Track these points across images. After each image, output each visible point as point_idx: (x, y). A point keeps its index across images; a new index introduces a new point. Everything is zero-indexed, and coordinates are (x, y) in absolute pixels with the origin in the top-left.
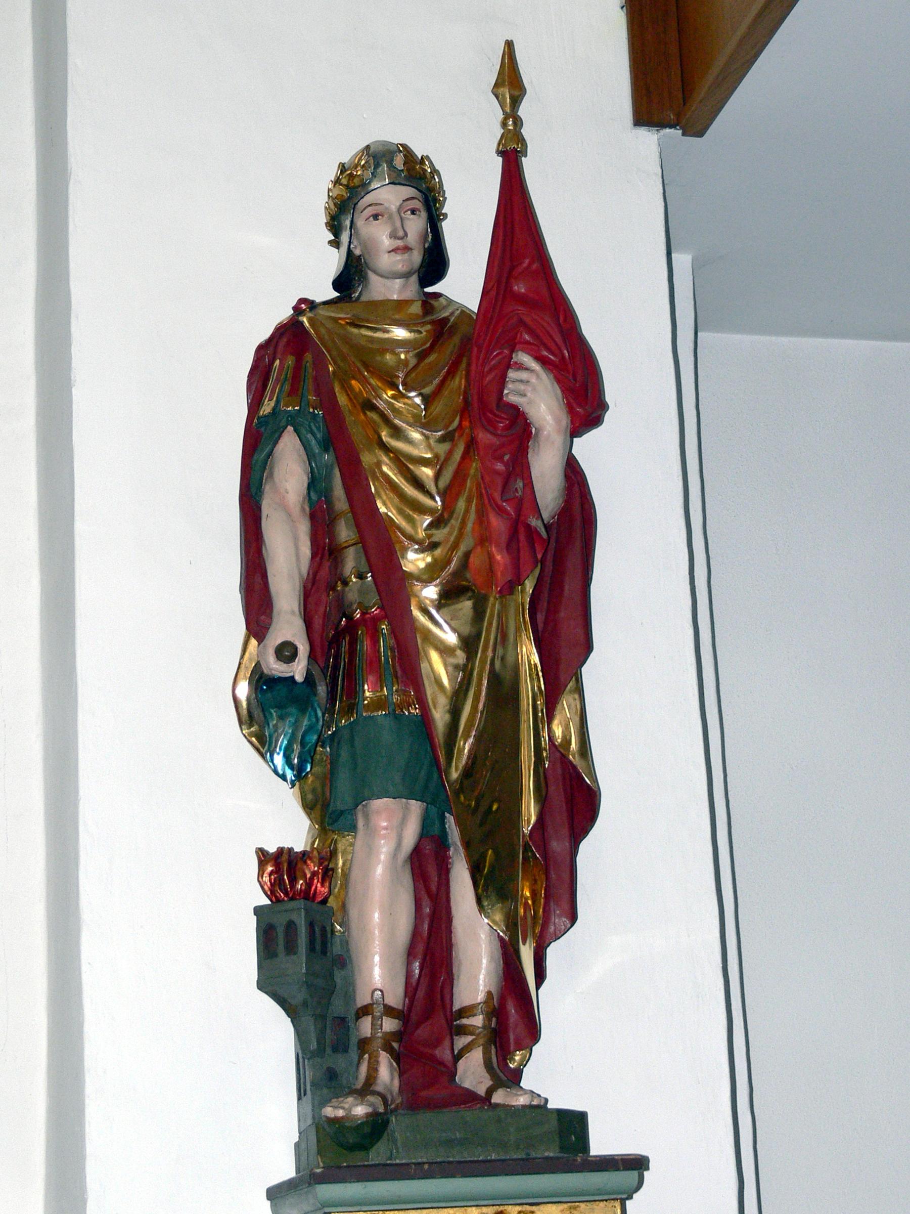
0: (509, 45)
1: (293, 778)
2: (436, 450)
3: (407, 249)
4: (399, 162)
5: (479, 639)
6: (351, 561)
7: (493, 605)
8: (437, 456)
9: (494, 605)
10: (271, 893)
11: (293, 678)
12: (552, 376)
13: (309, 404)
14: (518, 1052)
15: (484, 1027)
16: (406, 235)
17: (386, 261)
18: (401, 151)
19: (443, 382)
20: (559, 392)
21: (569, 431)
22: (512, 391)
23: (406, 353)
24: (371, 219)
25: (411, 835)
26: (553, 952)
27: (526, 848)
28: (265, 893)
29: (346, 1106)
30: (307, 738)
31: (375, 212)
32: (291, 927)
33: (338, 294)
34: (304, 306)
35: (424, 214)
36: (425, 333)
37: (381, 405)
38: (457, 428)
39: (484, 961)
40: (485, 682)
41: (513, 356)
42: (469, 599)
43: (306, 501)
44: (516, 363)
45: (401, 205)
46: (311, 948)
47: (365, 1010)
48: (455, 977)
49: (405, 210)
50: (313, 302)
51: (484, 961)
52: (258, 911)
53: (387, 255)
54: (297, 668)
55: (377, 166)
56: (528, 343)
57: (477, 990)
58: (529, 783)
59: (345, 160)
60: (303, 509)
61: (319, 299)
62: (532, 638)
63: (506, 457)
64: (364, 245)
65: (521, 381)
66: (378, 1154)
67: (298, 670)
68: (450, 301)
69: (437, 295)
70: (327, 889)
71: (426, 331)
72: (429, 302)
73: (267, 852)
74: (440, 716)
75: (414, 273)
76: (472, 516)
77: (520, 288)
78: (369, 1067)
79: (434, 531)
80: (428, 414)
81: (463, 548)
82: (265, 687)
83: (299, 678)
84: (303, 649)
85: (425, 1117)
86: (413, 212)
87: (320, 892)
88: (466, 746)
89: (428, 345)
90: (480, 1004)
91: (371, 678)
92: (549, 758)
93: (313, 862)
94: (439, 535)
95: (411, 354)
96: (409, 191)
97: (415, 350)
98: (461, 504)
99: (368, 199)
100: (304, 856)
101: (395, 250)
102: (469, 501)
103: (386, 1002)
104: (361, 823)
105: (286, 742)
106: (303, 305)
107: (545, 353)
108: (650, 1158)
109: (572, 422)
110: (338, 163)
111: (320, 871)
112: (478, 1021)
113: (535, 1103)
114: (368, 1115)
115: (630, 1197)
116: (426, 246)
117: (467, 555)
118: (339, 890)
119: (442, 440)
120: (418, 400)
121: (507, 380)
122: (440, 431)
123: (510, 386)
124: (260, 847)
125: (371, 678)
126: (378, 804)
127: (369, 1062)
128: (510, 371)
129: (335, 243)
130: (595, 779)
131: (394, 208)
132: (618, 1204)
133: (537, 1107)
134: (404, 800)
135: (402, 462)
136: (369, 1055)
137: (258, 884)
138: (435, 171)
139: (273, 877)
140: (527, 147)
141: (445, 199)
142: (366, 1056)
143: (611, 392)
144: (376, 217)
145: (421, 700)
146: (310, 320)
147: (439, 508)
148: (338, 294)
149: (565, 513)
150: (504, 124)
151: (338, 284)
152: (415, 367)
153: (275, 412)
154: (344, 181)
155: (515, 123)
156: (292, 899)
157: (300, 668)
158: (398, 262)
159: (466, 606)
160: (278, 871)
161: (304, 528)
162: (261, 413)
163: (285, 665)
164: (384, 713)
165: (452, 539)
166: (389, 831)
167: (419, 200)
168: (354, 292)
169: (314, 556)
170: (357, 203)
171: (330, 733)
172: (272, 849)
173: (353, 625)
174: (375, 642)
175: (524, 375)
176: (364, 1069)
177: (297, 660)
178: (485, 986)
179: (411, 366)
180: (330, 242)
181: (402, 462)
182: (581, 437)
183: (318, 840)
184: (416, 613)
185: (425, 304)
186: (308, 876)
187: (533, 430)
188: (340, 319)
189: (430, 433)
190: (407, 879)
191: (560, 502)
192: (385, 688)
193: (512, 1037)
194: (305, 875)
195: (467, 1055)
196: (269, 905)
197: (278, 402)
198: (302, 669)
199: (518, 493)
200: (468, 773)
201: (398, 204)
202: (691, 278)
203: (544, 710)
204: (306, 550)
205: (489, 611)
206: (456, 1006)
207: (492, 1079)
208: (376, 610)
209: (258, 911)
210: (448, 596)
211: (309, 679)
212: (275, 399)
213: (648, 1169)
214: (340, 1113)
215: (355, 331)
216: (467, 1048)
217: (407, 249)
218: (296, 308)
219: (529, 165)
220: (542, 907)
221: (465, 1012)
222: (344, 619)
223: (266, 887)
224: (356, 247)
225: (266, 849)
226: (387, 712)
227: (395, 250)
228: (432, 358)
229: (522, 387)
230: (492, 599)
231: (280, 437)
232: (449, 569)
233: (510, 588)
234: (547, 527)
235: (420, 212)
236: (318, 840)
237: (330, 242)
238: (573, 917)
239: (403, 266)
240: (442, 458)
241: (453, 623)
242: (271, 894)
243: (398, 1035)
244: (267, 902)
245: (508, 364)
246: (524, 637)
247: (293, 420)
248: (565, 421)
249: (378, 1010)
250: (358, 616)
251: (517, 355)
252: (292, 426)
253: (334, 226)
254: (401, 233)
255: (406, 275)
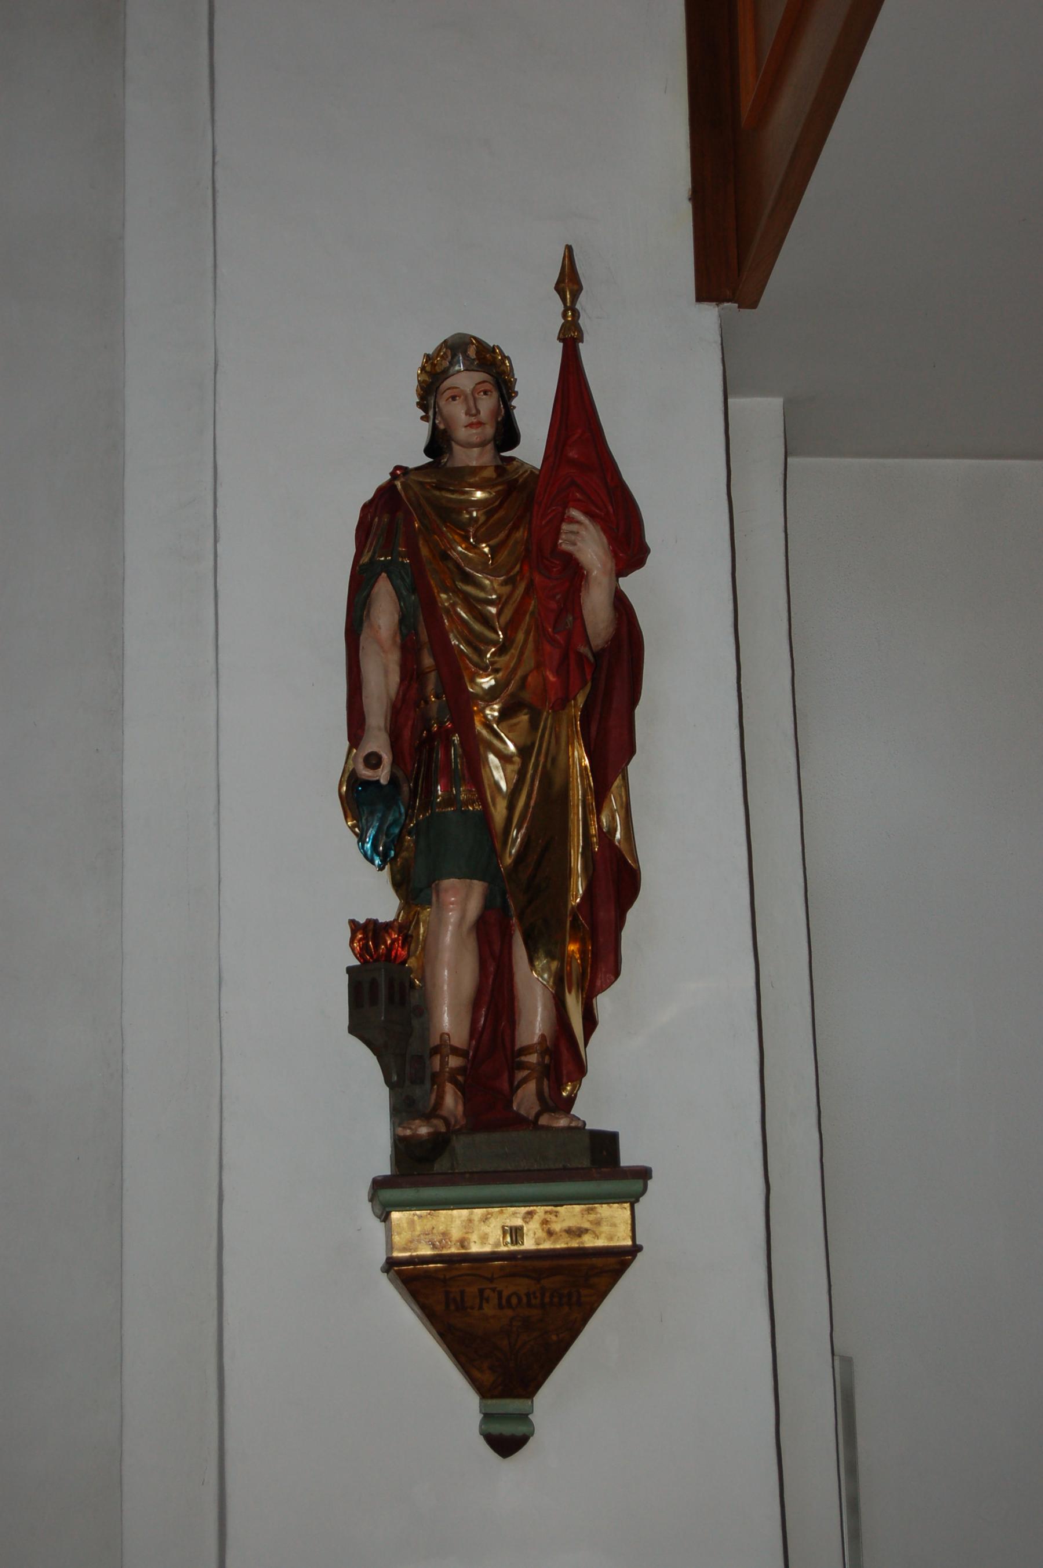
0: (569, 249)
1: (380, 863)
2: (498, 592)
3: (480, 424)
4: (472, 352)
5: (533, 749)
6: (432, 682)
7: (546, 718)
8: (499, 597)
9: (547, 719)
10: (360, 956)
11: (378, 781)
12: (599, 527)
13: (400, 554)
14: (570, 1083)
15: (538, 1063)
16: (478, 412)
17: (462, 433)
18: (473, 344)
19: (508, 536)
20: (605, 540)
21: (614, 572)
22: (566, 540)
23: (477, 511)
24: (450, 399)
25: (474, 907)
26: (604, 1002)
27: (575, 919)
28: (356, 955)
29: (413, 1127)
30: (392, 831)
31: (453, 394)
32: (374, 984)
33: (430, 460)
34: (400, 472)
35: (495, 395)
36: (494, 494)
37: (455, 555)
38: (518, 572)
39: (540, 1010)
40: (537, 783)
41: (566, 511)
42: (525, 714)
43: (398, 634)
44: (569, 517)
45: (474, 388)
46: (390, 999)
47: (436, 1050)
48: (517, 1023)
49: (479, 391)
50: (406, 468)
51: (540, 1010)
52: (350, 970)
53: (463, 429)
54: (382, 774)
55: (454, 356)
56: (579, 500)
57: (533, 1033)
58: (578, 864)
59: (430, 352)
60: (394, 642)
61: (411, 465)
62: (582, 745)
63: (558, 597)
64: (445, 420)
65: (572, 532)
66: (442, 1165)
67: (383, 775)
68: (523, 464)
69: (512, 459)
70: (406, 953)
71: (495, 492)
72: (504, 466)
73: (358, 923)
74: (499, 811)
75: (489, 442)
76: (530, 645)
77: (573, 454)
78: (437, 1096)
79: (496, 659)
80: (494, 562)
81: (520, 673)
82: (360, 788)
83: (384, 781)
84: (387, 758)
85: (480, 1138)
86: (485, 393)
87: (400, 954)
88: (517, 835)
89: (497, 503)
90: (535, 1044)
91: (443, 781)
92: (599, 844)
93: (394, 931)
94: (502, 660)
95: (481, 512)
96: (480, 376)
97: (485, 508)
98: (520, 636)
99: (448, 383)
100: (387, 926)
101: (470, 425)
102: (527, 633)
103: (452, 1043)
104: (434, 899)
105: (374, 832)
106: (398, 472)
107: (593, 508)
108: (653, 1169)
109: (617, 565)
110: (423, 354)
111: (400, 938)
112: (533, 1058)
113: (573, 1124)
114: (429, 1134)
115: (637, 1201)
116: (499, 419)
117: (524, 678)
118: (420, 953)
119: (505, 583)
120: (486, 550)
121: (562, 531)
122: (502, 576)
123: (563, 536)
124: (352, 918)
125: (443, 781)
126: (447, 883)
127: (437, 1092)
128: (563, 524)
129: (425, 418)
130: (636, 861)
131: (468, 390)
132: (627, 1205)
133: (576, 1128)
134: (468, 880)
135: (472, 604)
136: (438, 1086)
137: (349, 948)
138: (505, 357)
139: (361, 943)
140: (583, 334)
141: (516, 380)
142: (435, 1087)
143: (651, 536)
144: (454, 398)
145: (482, 799)
146: (402, 484)
147: (501, 640)
148: (430, 460)
149: (615, 640)
150: (564, 315)
151: (428, 451)
152: (484, 524)
153: (372, 561)
154: (428, 369)
155: (573, 315)
156: (377, 960)
157: (383, 774)
158: (473, 435)
159: (524, 718)
160: (365, 938)
161: (394, 658)
162: (361, 562)
163: (371, 771)
164: (452, 809)
165: (512, 665)
166: (455, 906)
167: (490, 383)
168: (443, 459)
169: (402, 679)
170: (439, 387)
171: (412, 825)
172: (362, 921)
173: (431, 736)
174: (448, 752)
175: (574, 527)
176: (433, 1097)
177: (382, 767)
178: (540, 1030)
179: (480, 522)
180: (422, 418)
181: (472, 604)
182: (626, 576)
183: (402, 912)
184: (479, 727)
185: (497, 468)
186: (389, 942)
187: (585, 572)
188: (427, 483)
189: (494, 578)
190: (472, 944)
191: (611, 630)
192: (454, 789)
193: (565, 1072)
194: (386, 942)
195: (524, 1086)
196: (359, 965)
197: (374, 553)
198: (386, 773)
199: (567, 626)
200: (520, 858)
201: (472, 387)
202: (783, 418)
203: (594, 804)
204: (395, 678)
205: (542, 724)
206: (517, 1047)
207: (540, 1106)
208: (449, 724)
209: (350, 970)
210: (505, 714)
211: (393, 780)
212: (372, 551)
213: (650, 1177)
214: (408, 1132)
215: (437, 493)
216: (525, 1081)
217: (480, 424)
218: (393, 474)
219: (585, 350)
220: (589, 966)
221: (526, 1050)
222: (425, 732)
223: (356, 952)
224: (440, 423)
225: (357, 920)
226: (455, 809)
227: (470, 425)
228: (501, 513)
229: (573, 537)
230: (545, 713)
231: (375, 582)
232: (507, 691)
233: (563, 702)
234: (595, 655)
235: (491, 392)
236: (402, 912)
237: (422, 418)
238: (617, 973)
239: (477, 438)
240: (503, 600)
241: (510, 735)
242: (360, 956)
243: (462, 1070)
244: (357, 963)
245: (563, 518)
246: (576, 744)
247: (386, 567)
248: (610, 564)
249: (446, 1050)
250: (436, 729)
251: (569, 511)
252: (385, 572)
253: (423, 405)
254: (474, 412)
255: (482, 444)
